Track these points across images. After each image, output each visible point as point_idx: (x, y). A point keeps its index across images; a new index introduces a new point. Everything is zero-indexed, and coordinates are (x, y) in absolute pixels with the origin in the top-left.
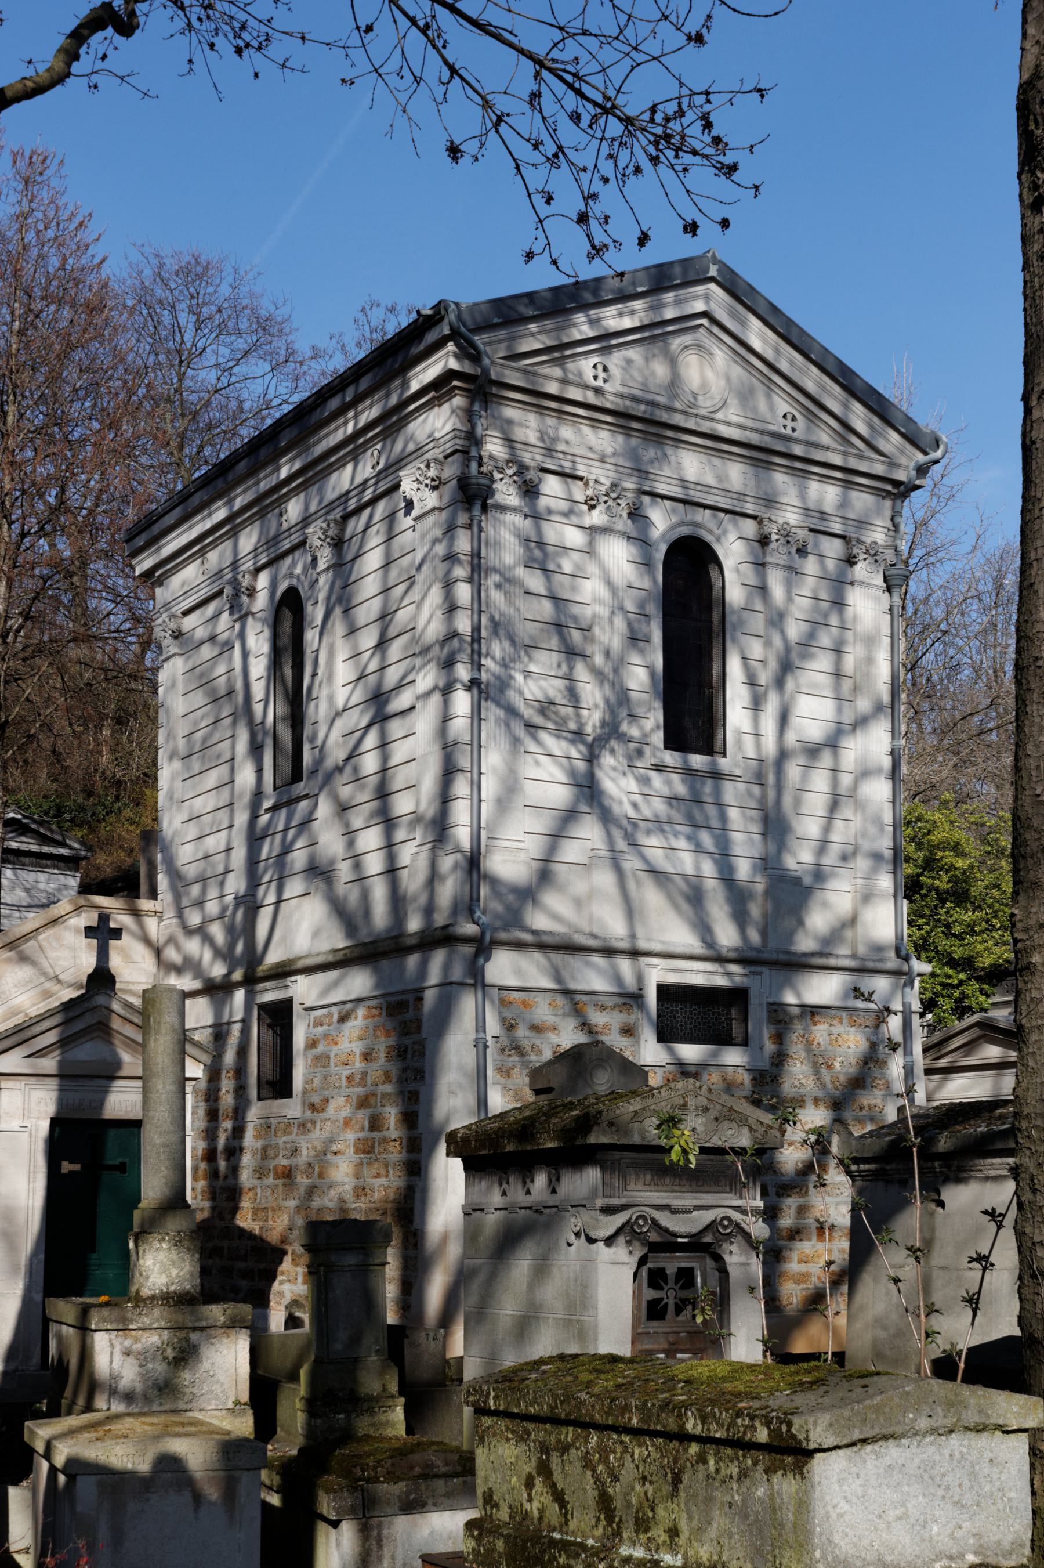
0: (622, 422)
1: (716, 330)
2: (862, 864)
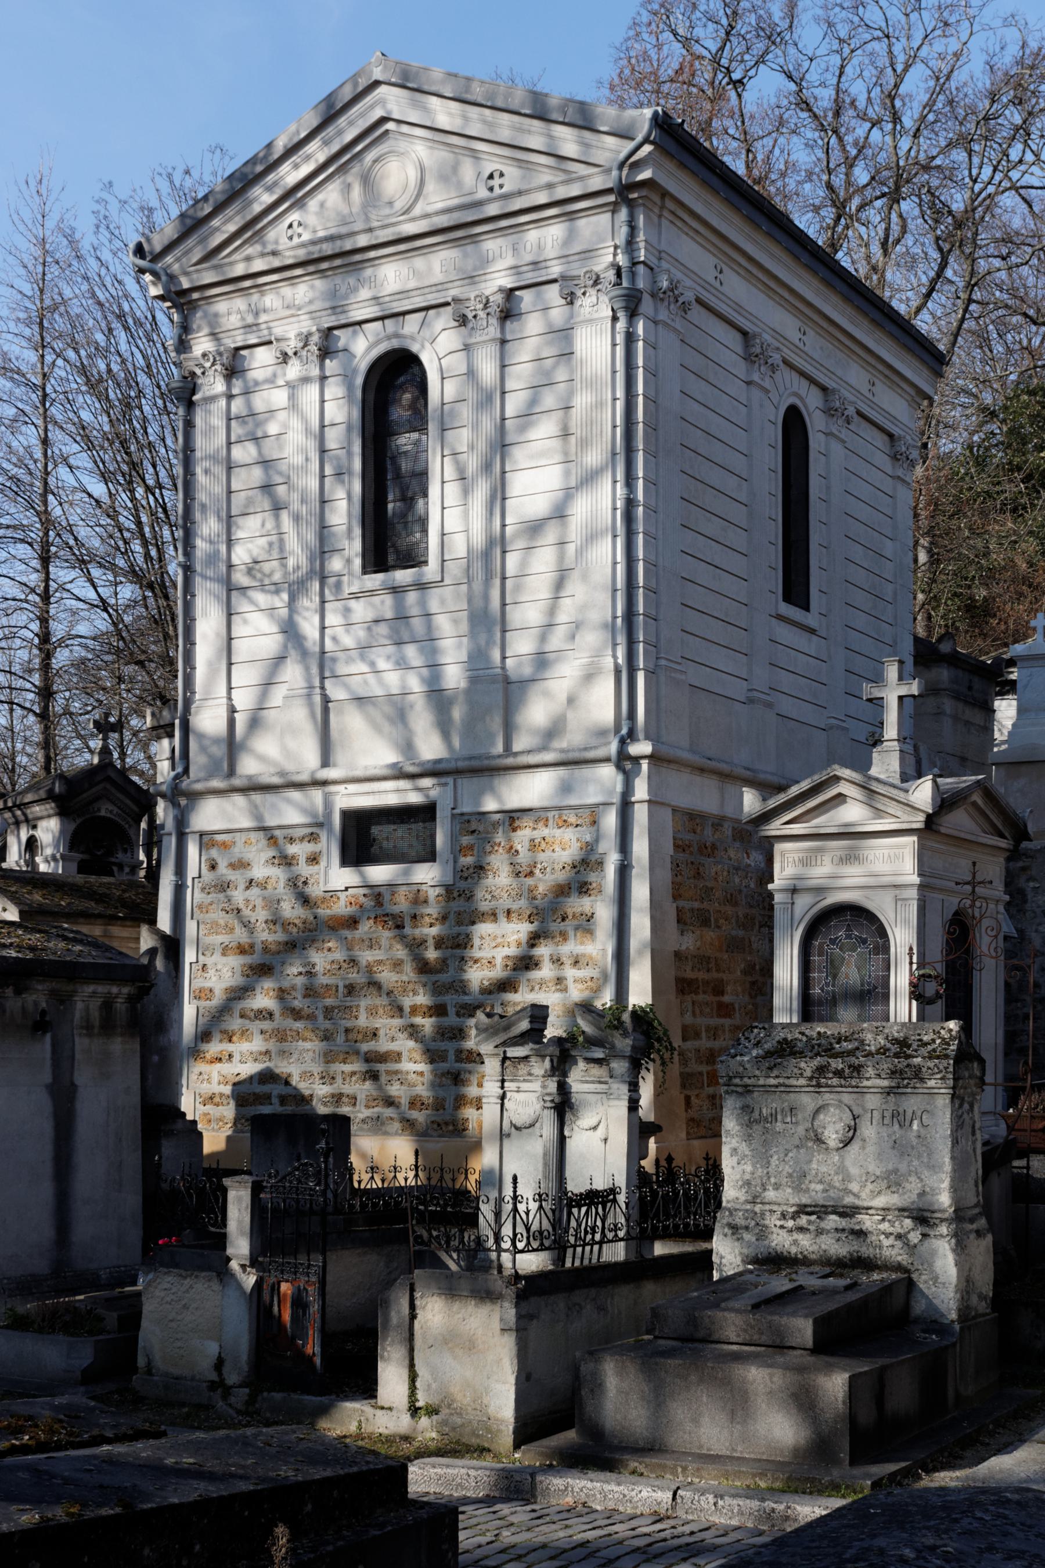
0: (311, 268)
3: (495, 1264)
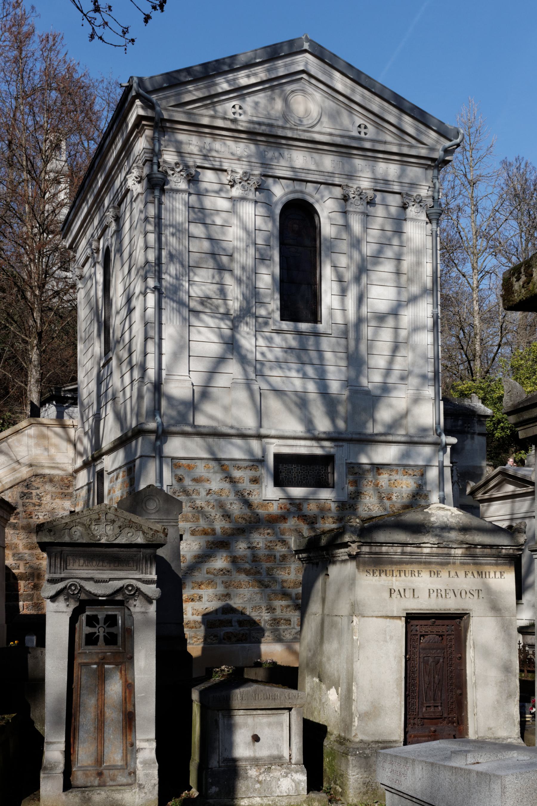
1: (313, 81)
2: (413, 381)
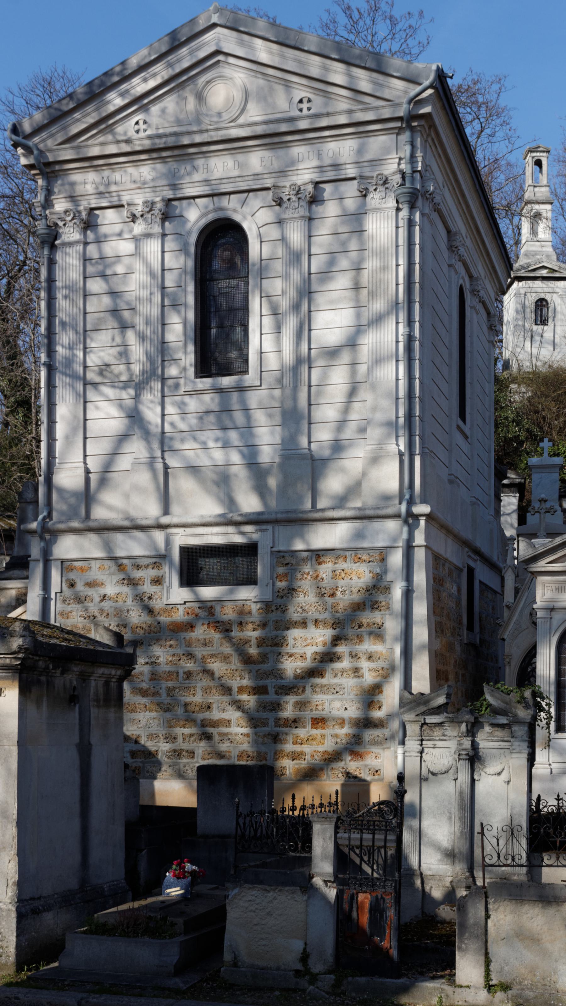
0: (154, 155)
2: (375, 433)
3: (418, 872)
